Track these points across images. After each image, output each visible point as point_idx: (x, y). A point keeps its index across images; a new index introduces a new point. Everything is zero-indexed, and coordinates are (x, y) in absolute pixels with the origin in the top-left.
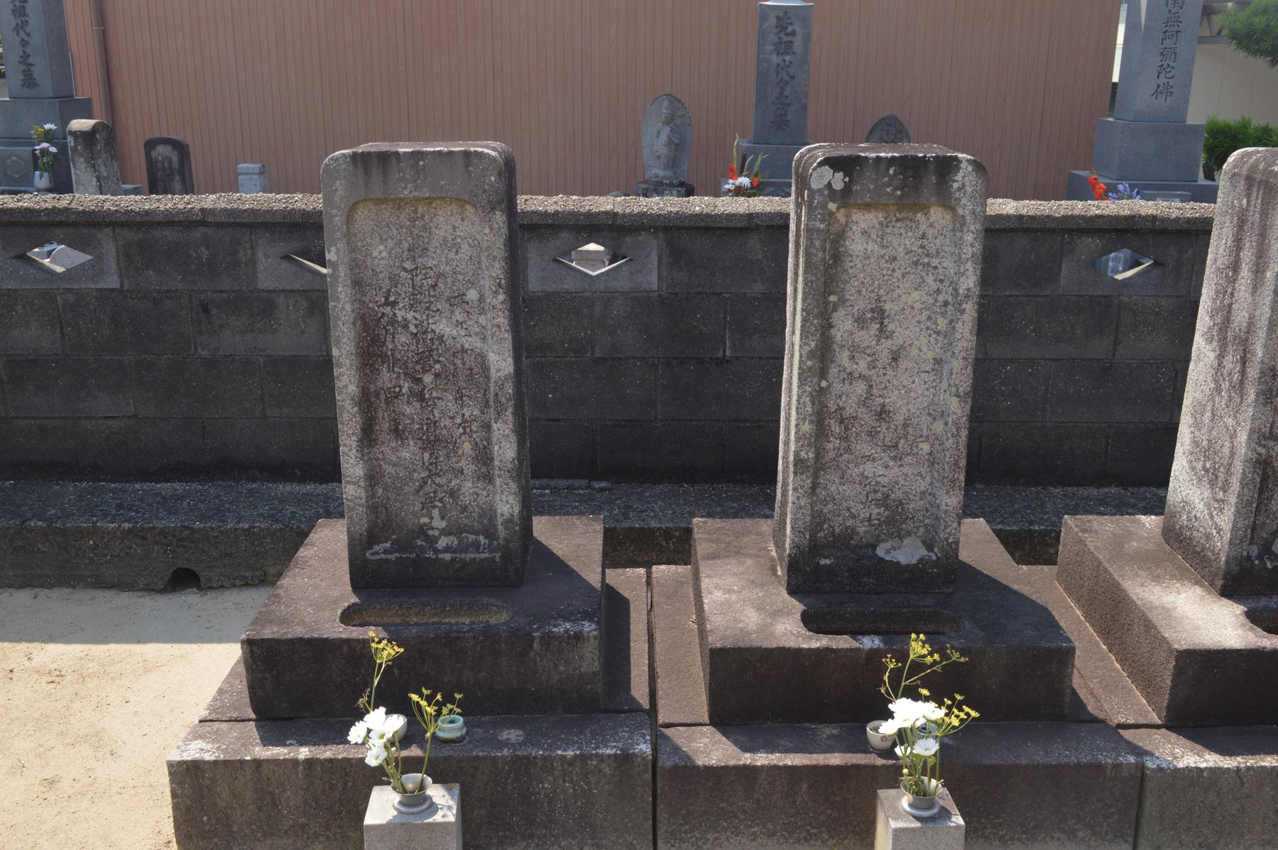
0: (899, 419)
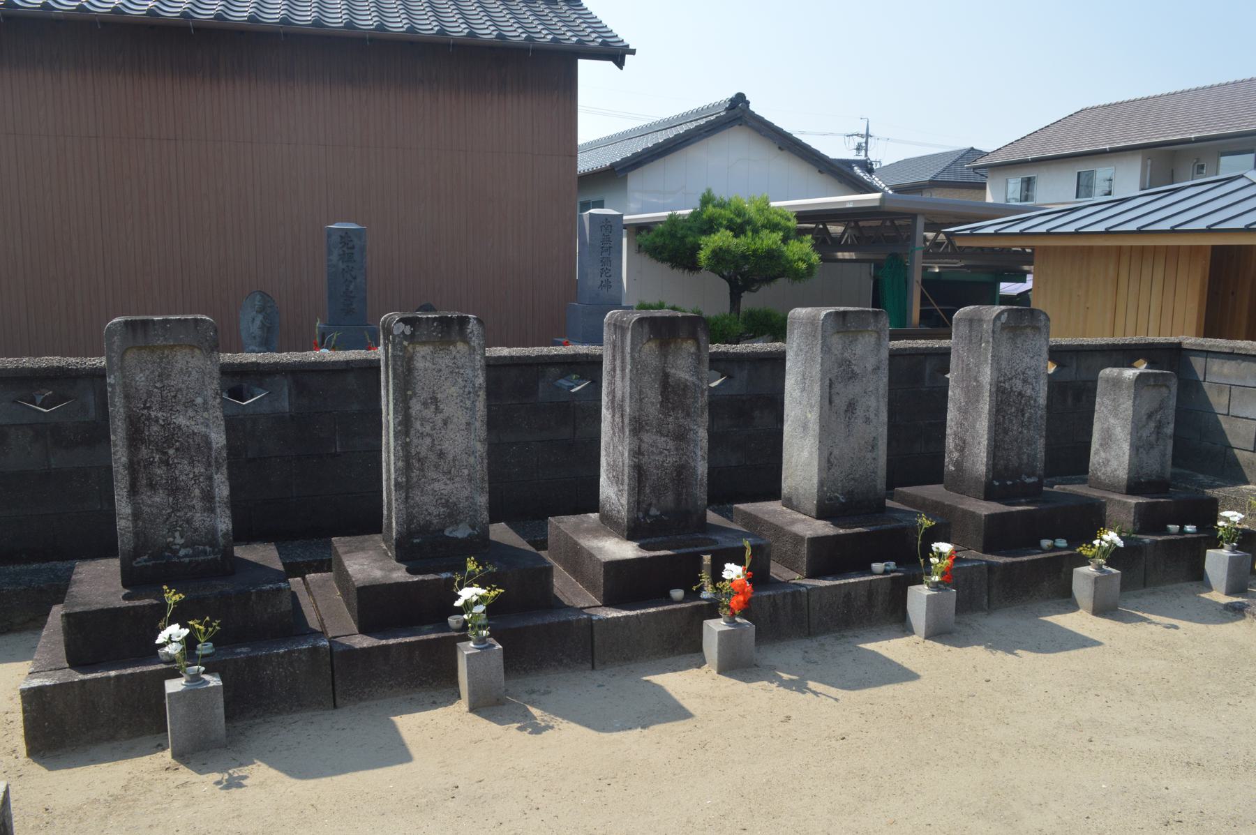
0: (451, 457)
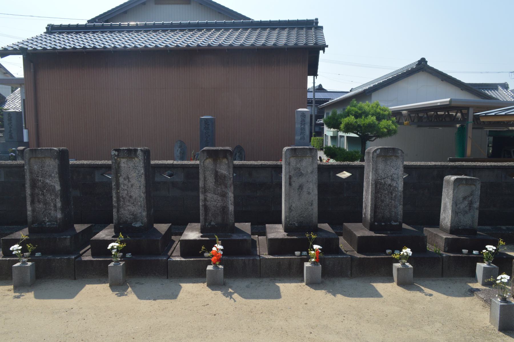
0: (134, 198)
